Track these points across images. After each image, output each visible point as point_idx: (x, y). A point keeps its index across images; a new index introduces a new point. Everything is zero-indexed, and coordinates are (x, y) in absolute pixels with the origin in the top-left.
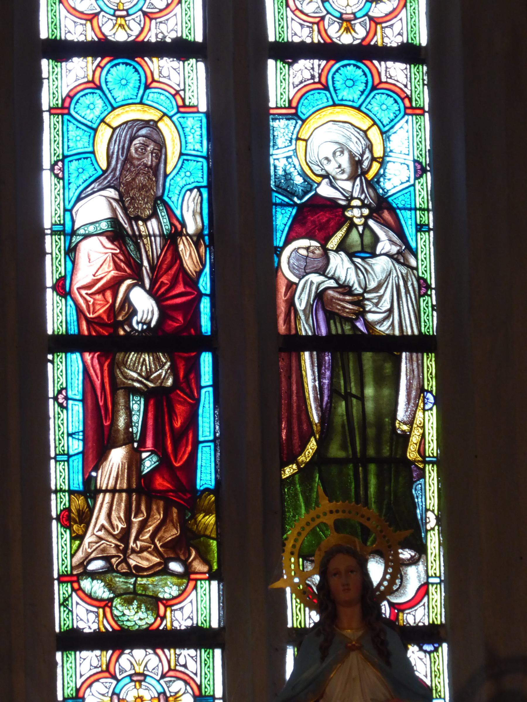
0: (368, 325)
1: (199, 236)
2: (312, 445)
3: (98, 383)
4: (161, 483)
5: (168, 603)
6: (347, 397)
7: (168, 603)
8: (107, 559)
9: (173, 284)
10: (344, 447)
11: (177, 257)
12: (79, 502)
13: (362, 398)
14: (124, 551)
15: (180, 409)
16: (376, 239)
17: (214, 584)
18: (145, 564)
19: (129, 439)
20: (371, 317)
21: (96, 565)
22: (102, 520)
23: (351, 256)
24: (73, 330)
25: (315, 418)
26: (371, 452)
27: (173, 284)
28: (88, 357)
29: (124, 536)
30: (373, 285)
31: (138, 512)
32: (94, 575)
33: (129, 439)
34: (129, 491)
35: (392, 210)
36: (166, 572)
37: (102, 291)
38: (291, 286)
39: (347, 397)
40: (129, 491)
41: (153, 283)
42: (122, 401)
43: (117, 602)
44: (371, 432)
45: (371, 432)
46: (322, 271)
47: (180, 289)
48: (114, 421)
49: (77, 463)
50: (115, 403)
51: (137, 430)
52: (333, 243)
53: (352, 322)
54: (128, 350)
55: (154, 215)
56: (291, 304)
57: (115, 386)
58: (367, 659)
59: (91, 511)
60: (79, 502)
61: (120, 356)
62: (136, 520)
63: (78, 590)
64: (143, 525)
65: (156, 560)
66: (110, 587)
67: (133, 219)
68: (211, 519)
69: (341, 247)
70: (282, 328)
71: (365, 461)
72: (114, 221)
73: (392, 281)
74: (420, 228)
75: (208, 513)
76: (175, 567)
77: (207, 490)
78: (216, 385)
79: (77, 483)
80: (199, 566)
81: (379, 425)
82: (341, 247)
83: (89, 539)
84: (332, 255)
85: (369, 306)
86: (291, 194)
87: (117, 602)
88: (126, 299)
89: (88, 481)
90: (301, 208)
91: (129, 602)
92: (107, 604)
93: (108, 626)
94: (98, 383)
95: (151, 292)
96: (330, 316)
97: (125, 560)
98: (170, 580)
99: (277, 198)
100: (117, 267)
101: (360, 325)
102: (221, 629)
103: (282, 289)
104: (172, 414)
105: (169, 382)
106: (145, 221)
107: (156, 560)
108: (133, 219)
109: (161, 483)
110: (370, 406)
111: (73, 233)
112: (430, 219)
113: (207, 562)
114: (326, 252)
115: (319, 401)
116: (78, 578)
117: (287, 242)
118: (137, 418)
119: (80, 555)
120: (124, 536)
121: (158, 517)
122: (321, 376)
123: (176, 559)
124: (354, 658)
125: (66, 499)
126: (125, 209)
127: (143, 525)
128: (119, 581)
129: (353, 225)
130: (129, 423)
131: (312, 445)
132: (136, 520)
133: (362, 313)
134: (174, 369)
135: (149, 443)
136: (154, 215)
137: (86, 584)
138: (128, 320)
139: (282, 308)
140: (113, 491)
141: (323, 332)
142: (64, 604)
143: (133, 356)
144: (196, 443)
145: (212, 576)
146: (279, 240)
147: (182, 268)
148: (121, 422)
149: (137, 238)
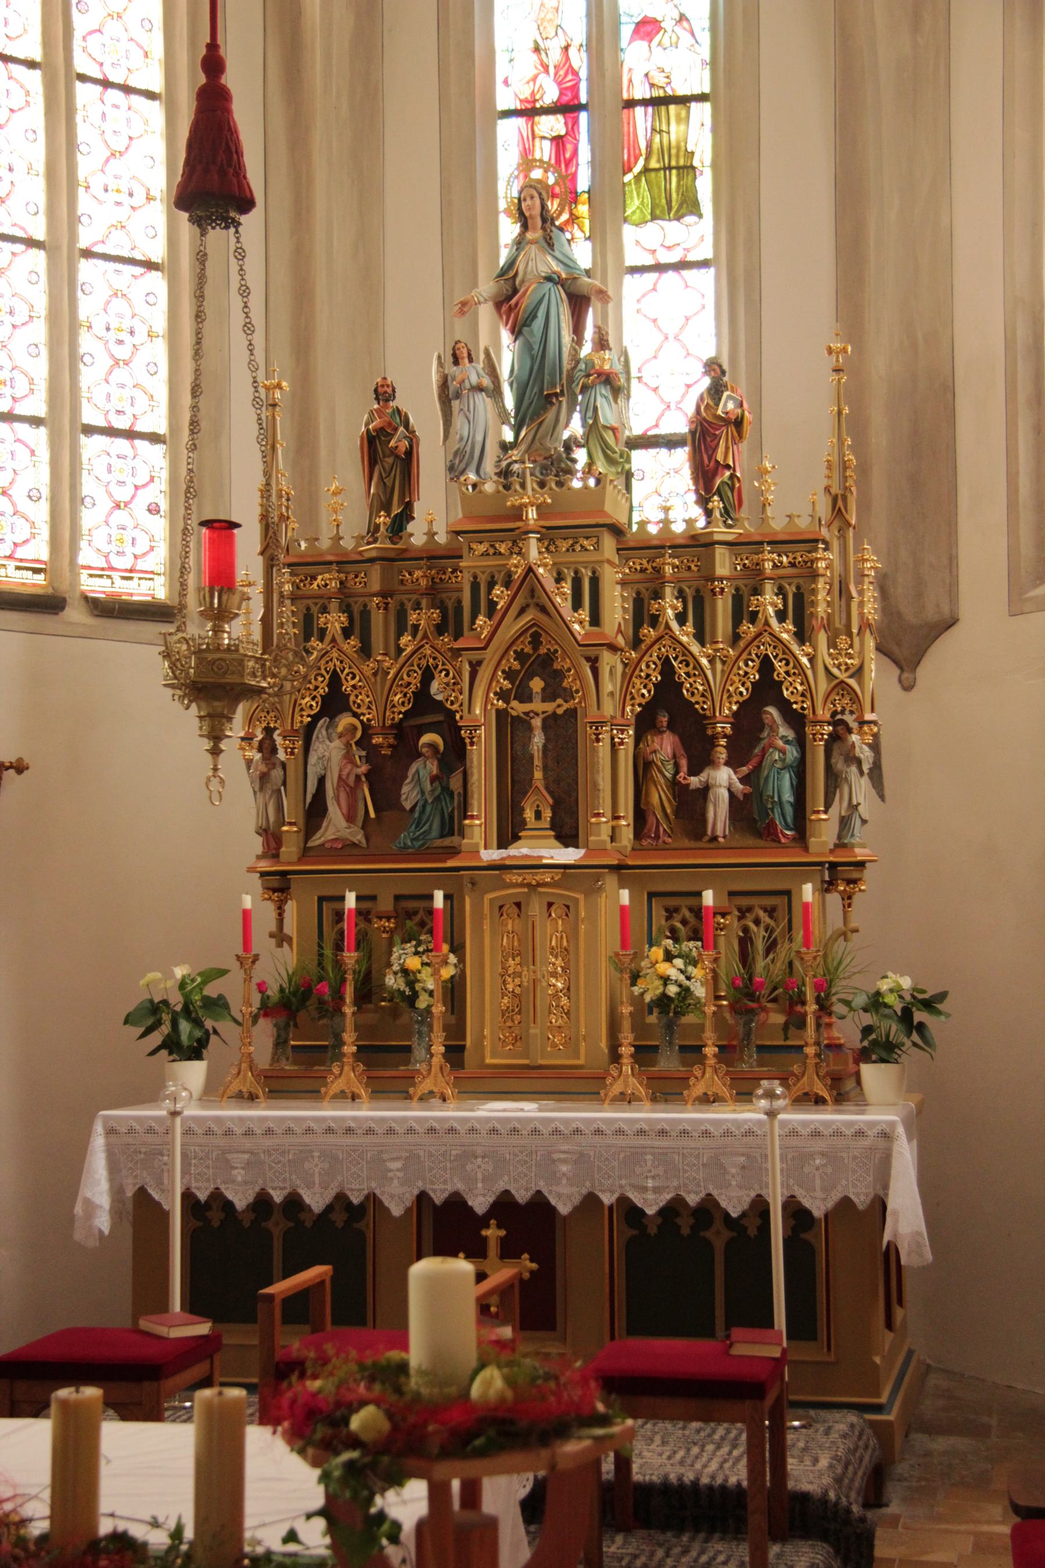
2: (641, 162)
6: (661, 132)
10: (658, 161)
15: (569, 147)
26: (673, 163)
27: (566, 75)
45: (673, 151)
47: (570, 77)
104: (564, 150)
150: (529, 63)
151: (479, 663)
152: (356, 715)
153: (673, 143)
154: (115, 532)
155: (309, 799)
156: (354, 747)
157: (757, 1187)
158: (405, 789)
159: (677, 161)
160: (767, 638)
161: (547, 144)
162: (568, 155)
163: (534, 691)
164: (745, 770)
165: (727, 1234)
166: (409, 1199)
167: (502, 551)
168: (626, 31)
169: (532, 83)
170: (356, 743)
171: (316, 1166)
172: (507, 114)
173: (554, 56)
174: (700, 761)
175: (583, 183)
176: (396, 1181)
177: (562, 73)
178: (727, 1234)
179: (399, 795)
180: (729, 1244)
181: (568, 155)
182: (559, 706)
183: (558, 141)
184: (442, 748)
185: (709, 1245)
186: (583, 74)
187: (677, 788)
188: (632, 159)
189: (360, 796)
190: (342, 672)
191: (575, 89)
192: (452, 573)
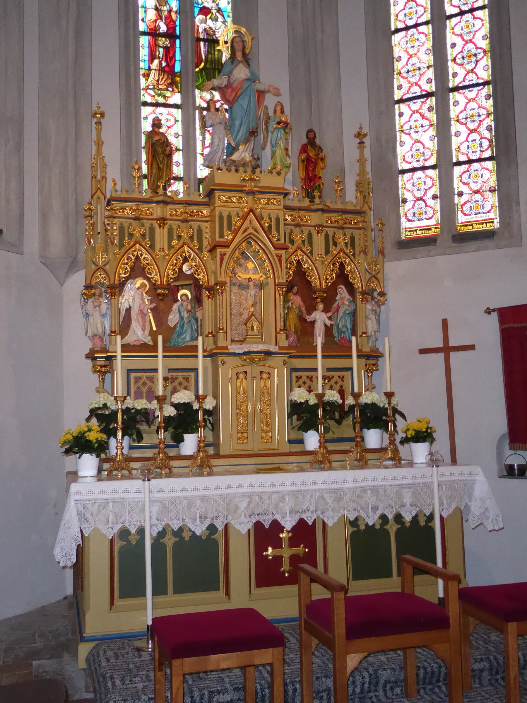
0: (216, 37)
1: (176, 12)
2: (203, 64)
3: (152, 44)
4: (167, 69)
5: (168, 98)
6: (211, 54)
7: (168, 98)
8: (154, 86)
9: (170, 22)
10: (210, 65)
11: (171, 16)
12: (147, 71)
13: (214, 54)
14: (158, 84)
15: (171, 52)
16: (218, 18)
17: (179, 94)
18: (163, 88)
19: (159, 58)
20: (217, 36)
21: (151, 87)
22: (153, 76)
23: (212, 21)
24: (146, 31)
25: (204, 58)
26: (216, 67)
27: (170, 22)
28: (149, 37)
29: (158, 81)
30: (217, 28)
31: (161, 75)
32: (150, 89)
33: (159, 58)
34: (159, 70)
35: (222, 12)
36: (168, 90)
37: (153, 22)
38: (198, 26)
39: (211, 54)
40: (159, 70)
41: (165, 21)
42: (157, 49)
43: (156, 96)
44: (216, 62)
45: (216, 62)
46: (206, 23)
47: (172, 23)
48: (155, 53)
49: (147, 62)
50: (156, 49)
51: (161, 56)
52: (208, 17)
53: (212, 36)
54: (159, 37)
55: (166, 5)
56: (198, 30)
57: (156, 45)
58: (244, 65)
59: (150, 74)
60: (147, 71)
61: (157, 38)
62: (161, 77)
63: (147, 92)
64: (162, 78)
65: (165, 87)
66: (155, 92)
67: (160, 6)
68: (178, 79)
69: (210, 18)
70: (196, 35)
71: (216, 69)
72: (156, 6)
73: (222, 27)
74: (229, 16)
75: (178, 77)
76: (170, 89)
77: (178, 72)
78: (180, 47)
79: (147, 68)
80: (176, 89)
81: (219, 61)
82: (210, 18)
83: (149, 80)
84: (208, 20)
85: (216, 33)
86: (198, 4)
87: (156, 96)
88: (159, 25)
89: (149, 67)
90: (201, 8)
91: (159, 96)
92: (153, 96)
93: (154, 101)
94: (152, 44)
95: (165, 23)
96: (207, 34)
97: (158, 86)
98: (169, 92)
99: (196, 5)
100: (157, 17)
101: (214, 37)
102: (181, 105)
103: (196, 27)
104: (169, 53)
105: (169, 45)
106: (163, 6)
107: (165, 87)
108: (160, 6)
109: (167, 69)
110: (216, 56)
111: (146, 7)
112: (231, 15)
113: (178, 89)
114: (206, 19)
115: (205, 54)
116: (146, 90)
117: (198, 15)
118: (161, 53)
119: (147, 84)
120: (158, 81)
121: (166, 77)
122: (205, 48)
123: (170, 87)
124: (241, 64)
125: (144, 70)
126: (159, 3)
127: (162, 78)
128: (157, 91)
129: (212, 14)
130: (159, 54)
131: (203, 64)
132: (161, 77)
133: (215, 34)
134: (170, 42)
135: (164, 59)
136: (166, 5)
137: (149, 91)
138: (159, 30)
139: (196, 31)
140: (155, 70)
141: (206, 37)
142: (143, 95)
143: (160, 38)
144: (175, 61)
145: (179, 92)
146: (196, 15)
147: (172, 19)
148: (157, 54)
149: (161, 10)
150: (152, 15)
151: (225, 254)
152: (148, 279)
153: (216, 59)
154: (466, 61)
155: (121, 319)
156: (144, 294)
157: (342, 511)
158: (170, 317)
159: (218, 67)
160: (342, 254)
161: (161, 50)
162: (171, 55)
163: (249, 268)
164: (329, 314)
165: (174, 540)
166: (250, 525)
167: (234, 201)
168: (197, 10)
169: (154, 23)
170: (146, 293)
171: (198, 509)
172: (144, 33)
173: (165, 14)
174: (311, 309)
175: (177, 69)
176: (243, 516)
177: (168, 21)
178: (174, 540)
179: (167, 319)
180: (175, 544)
181: (171, 55)
182: (261, 277)
183: (167, 50)
184: (190, 297)
185: (164, 546)
186: (178, 23)
187: (302, 320)
188: (199, 63)
189: (147, 319)
190: (141, 256)
191: (174, 28)
192: (196, 212)
